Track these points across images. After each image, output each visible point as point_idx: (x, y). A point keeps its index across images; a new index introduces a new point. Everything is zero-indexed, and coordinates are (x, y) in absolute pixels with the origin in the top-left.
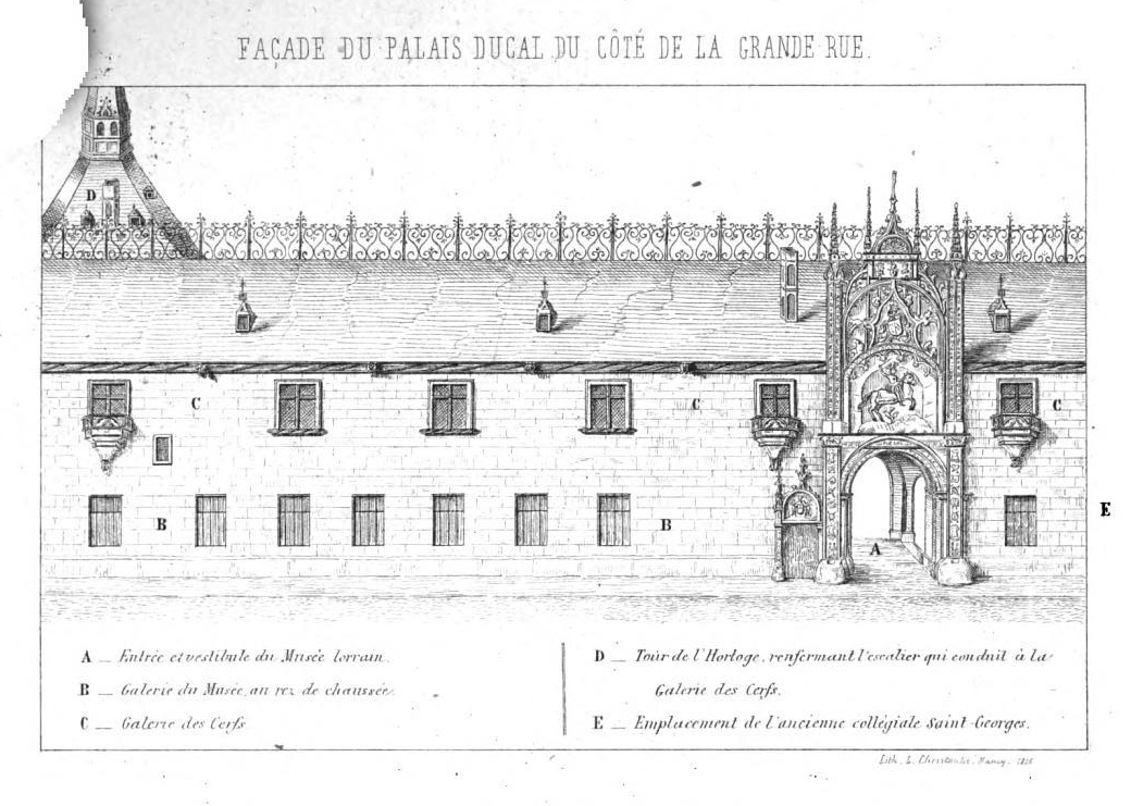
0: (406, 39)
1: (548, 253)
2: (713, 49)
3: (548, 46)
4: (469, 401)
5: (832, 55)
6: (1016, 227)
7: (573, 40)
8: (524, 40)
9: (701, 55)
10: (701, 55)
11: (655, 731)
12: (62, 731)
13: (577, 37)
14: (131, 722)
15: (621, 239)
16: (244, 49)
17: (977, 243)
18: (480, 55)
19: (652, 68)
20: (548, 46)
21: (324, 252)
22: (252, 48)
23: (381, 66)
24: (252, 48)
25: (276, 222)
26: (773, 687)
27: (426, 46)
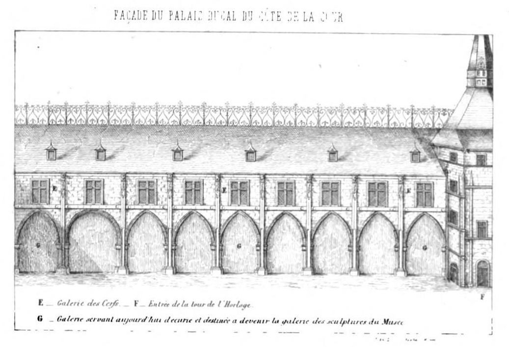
0: (177, 12)
1: (60, 121)
2: (122, 16)
3: (239, 16)
4: (248, 192)
5: (340, 21)
6: (184, 107)
7: (160, 12)
8: (190, 13)
9: (183, 19)
10: (183, 19)
11: (341, 325)
12: (27, 319)
13: (252, 12)
14: (62, 318)
15: (323, 114)
16: (116, 15)
17: (163, 115)
18: (245, 19)
19: (148, 24)
20: (239, 16)
21: (115, 120)
22: (119, 14)
23: (165, 23)
24: (119, 14)
25: (444, 108)
26: (117, 302)
27: (186, 15)
